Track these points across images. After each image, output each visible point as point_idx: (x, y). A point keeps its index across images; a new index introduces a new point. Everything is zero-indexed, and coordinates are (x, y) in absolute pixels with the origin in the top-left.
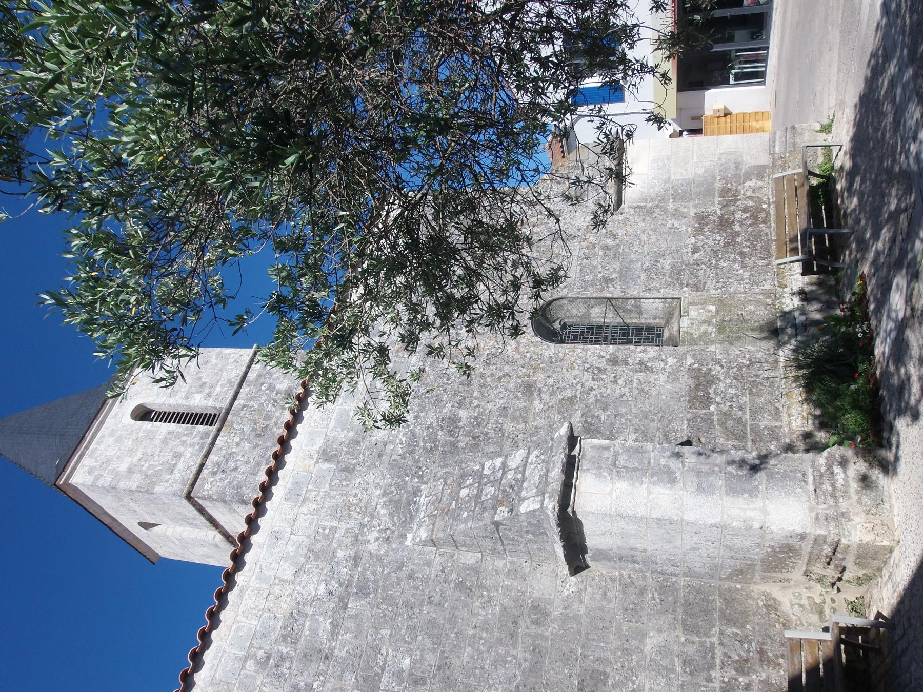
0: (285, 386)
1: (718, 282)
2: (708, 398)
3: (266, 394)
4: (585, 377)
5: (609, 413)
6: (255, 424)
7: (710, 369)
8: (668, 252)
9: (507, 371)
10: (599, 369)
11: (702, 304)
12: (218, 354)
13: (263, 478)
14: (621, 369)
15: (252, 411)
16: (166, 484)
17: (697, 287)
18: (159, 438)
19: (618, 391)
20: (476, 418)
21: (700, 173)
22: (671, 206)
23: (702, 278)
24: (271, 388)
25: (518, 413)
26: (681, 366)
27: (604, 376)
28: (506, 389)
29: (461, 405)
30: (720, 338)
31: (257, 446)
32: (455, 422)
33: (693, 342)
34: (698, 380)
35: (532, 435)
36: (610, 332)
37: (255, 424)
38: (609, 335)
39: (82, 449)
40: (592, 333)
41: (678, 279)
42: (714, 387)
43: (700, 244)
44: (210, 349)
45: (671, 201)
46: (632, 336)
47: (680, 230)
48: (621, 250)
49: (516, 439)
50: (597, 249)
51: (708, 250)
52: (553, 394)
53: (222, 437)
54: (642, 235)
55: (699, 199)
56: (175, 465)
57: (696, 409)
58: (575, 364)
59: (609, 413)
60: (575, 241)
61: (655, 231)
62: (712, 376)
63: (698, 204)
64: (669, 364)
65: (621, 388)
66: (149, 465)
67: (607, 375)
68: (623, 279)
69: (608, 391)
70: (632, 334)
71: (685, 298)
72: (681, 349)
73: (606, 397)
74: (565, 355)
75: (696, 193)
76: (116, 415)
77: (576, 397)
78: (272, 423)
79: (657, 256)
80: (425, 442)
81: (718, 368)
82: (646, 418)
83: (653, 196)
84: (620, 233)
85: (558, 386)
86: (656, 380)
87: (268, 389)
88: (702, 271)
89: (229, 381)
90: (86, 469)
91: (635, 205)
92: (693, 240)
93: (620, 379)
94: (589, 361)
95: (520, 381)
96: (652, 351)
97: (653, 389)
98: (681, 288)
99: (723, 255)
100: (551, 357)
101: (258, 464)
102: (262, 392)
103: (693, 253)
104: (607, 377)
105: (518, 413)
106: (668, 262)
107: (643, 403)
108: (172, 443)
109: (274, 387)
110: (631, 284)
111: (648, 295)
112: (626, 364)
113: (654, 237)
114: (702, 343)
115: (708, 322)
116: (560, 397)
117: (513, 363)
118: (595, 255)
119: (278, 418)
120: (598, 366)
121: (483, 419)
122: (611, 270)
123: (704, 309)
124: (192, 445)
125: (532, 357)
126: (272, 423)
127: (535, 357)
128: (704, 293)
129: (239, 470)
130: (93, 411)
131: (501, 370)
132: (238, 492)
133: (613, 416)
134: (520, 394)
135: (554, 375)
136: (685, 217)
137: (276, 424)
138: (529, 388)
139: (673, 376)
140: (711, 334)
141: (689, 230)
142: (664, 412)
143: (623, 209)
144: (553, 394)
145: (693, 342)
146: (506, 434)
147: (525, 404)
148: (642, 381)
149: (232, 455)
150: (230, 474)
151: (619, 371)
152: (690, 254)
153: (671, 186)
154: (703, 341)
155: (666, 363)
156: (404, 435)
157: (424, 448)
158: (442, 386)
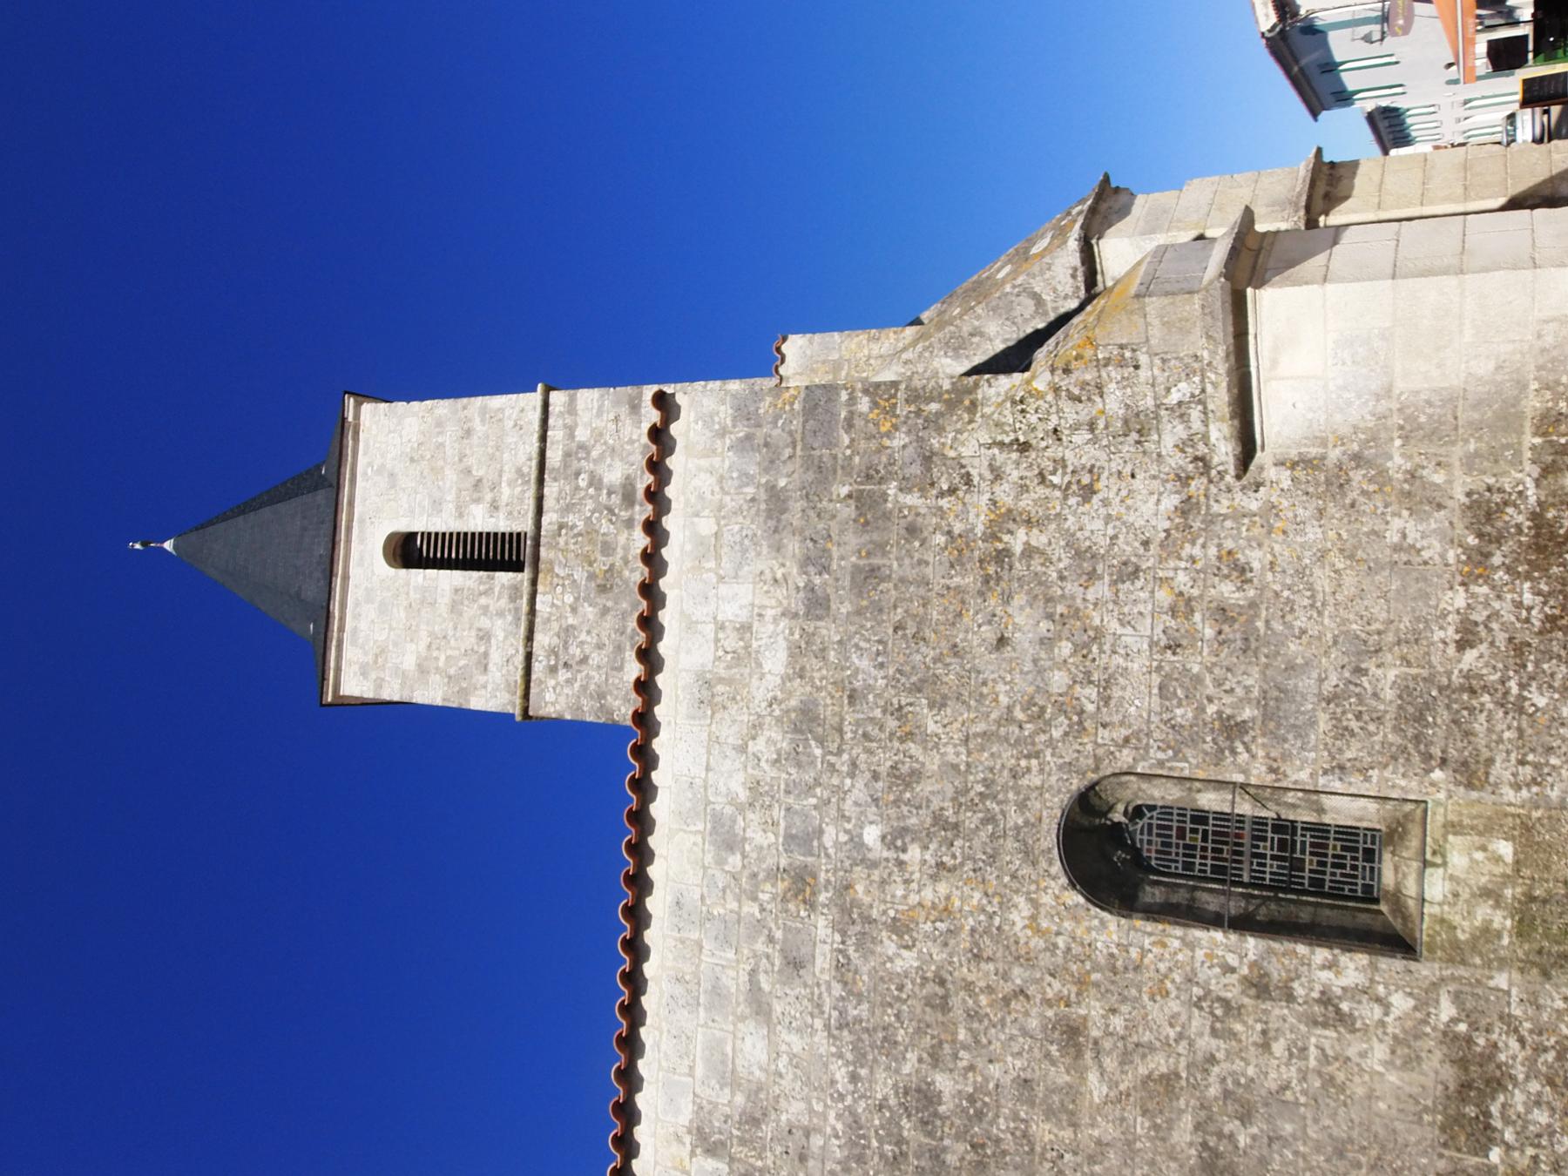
0: (619, 475)
1: (1522, 762)
2: (1488, 1127)
3: (591, 497)
4: (1194, 1023)
5: (1255, 1130)
6: (591, 565)
7: (1495, 1045)
8: (1390, 638)
9: (1018, 981)
10: (1225, 1003)
11: (1480, 834)
12: (484, 410)
13: (634, 669)
14: (1279, 1010)
15: (576, 536)
16: (483, 692)
17: (1471, 773)
18: (444, 602)
19: (1273, 1075)
20: (971, 1099)
21: (1481, 372)
22: (1397, 463)
23: (1481, 741)
24: (595, 482)
25: (1056, 1098)
26: (1425, 1022)
27: (1238, 1027)
28: (1025, 1032)
29: (935, 1059)
30: (1520, 953)
31: (605, 611)
32: (931, 1102)
33: (1456, 953)
34: (1466, 1070)
35: (1092, 1160)
36: (1247, 832)
37: (591, 565)
38: (1246, 841)
39: (335, 634)
40: (1205, 832)
41: (1417, 739)
42: (1501, 1098)
43: (1479, 616)
44: (465, 400)
45: (1398, 442)
46: (1303, 852)
47: (1426, 554)
48: (1260, 624)
49: (1059, 1163)
50: (1197, 617)
51: (1501, 638)
52: (1125, 1059)
53: (544, 594)
54: (1317, 572)
55: (1480, 439)
56: (486, 655)
57: (1459, 1150)
58: (1169, 985)
59: (1255, 1130)
60: (1139, 584)
61: (1351, 557)
62: (1499, 1067)
63: (1477, 454)
64: (1395, 1013)
65: (1277, 1070)
66: (447, 658)
67: (1245, 1023)
68: (1272, 725)
69: (1251, 1071)
70: (1303, 843)
71: (1438, 803)
72: (1426, 970)
73: (1247, 1087)
74: (1144, 952)
75: (1470, 423)
76: (362, 559)
77: (1178, 1076)
78: (617, 560)
79: (1363, 651)
80: (880, 1140)
81: (1514, 1044)
82: (1340, 1154)
83: (1345, 430)
84: (1256, 558)
85: (1135, 1038)
86: (1363, 1055)
87: (590, 484)
88: (1482, 718)
89: (519, 472)
90: (356, 668)
91: (1293, 454)
92: (1460, 599)
93: (1276, 1039)
94: (1201, 977)
95: (1050, 1013)
96: (1353, 968)
97: (1357, 1079)
98: (1428, 771)
99: (1537, 663)
100: (1112, 955)
101: (619, 649)
102: (583, 493)
103: (1462, 645)
104: (1247, 1030)
105: (1056, 1098)
106: (1392, 674)
107: (1334, 1116)
108: (470, 611)
109: (601, 480)
110: (1292, 744)
111: (1337, 786)
112: (1290, 997)
113: (1349, 579)
114: (1478, 961)
115: (1489, 894)
116: (1143, 1071)
117: (1028, 960)
118: (1194, 635)
119: (626, 549)
120: (1224, 994)
121: (985, 1104)
122: (1239, 691)
123: (1484, 848)
124: (500, 614)
125: (1069, 949)
126: (617, 560)
127: (1076, 949)
128: (1486, 796)
129: (590, 662)
130: (322, 550)
131: (1006, 977)
132: (602, 706)
133: (1265, 1140)
134: (1054, 1049)
135: (1125, 1008)
136: (1440, 506)
137: (626, 562)
138: (1071, 1034)
139: (1406, 1049)
140: (1499, 935)
141: (1451, 556)
142: (1383, 1147)
143: (1261, 468)
144: (1125, 1059)
145: (1456, 953)
146: (1038, 1149)
147: (1067, 1078)
148: (1330, 1052)
149: (568, 631)
150: (579, 671)
151: (1272, 1018)
152: (1451, 650)
153: (1395, 406)
154: (1481, 955)
155: (1386, 1007)
156: (839, 1117)
157: (882, 1156)
158: (890, 1005)
